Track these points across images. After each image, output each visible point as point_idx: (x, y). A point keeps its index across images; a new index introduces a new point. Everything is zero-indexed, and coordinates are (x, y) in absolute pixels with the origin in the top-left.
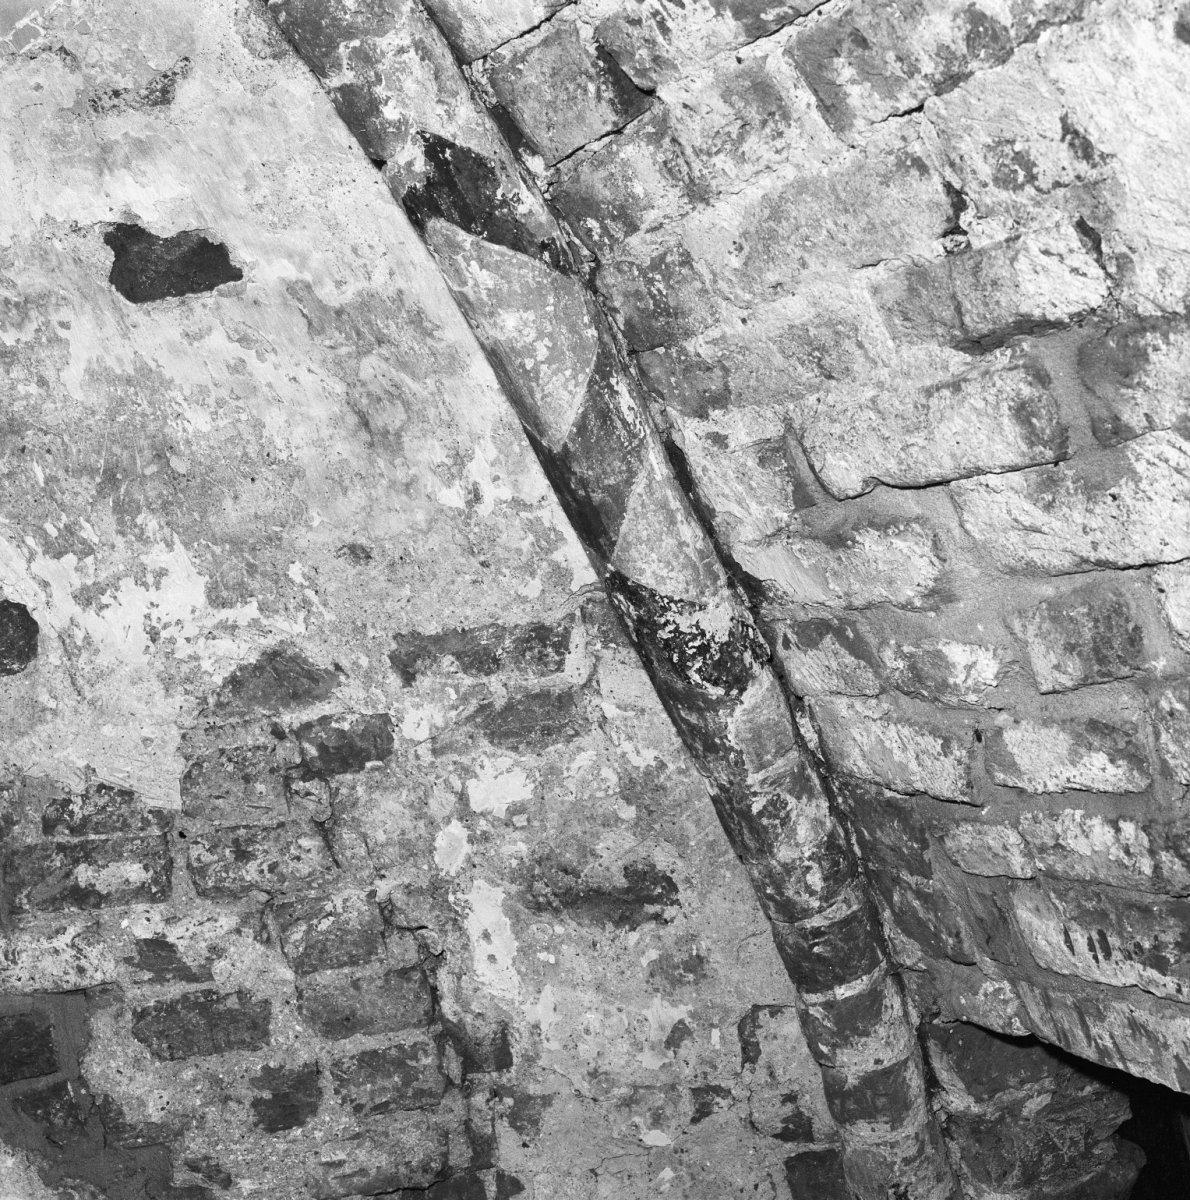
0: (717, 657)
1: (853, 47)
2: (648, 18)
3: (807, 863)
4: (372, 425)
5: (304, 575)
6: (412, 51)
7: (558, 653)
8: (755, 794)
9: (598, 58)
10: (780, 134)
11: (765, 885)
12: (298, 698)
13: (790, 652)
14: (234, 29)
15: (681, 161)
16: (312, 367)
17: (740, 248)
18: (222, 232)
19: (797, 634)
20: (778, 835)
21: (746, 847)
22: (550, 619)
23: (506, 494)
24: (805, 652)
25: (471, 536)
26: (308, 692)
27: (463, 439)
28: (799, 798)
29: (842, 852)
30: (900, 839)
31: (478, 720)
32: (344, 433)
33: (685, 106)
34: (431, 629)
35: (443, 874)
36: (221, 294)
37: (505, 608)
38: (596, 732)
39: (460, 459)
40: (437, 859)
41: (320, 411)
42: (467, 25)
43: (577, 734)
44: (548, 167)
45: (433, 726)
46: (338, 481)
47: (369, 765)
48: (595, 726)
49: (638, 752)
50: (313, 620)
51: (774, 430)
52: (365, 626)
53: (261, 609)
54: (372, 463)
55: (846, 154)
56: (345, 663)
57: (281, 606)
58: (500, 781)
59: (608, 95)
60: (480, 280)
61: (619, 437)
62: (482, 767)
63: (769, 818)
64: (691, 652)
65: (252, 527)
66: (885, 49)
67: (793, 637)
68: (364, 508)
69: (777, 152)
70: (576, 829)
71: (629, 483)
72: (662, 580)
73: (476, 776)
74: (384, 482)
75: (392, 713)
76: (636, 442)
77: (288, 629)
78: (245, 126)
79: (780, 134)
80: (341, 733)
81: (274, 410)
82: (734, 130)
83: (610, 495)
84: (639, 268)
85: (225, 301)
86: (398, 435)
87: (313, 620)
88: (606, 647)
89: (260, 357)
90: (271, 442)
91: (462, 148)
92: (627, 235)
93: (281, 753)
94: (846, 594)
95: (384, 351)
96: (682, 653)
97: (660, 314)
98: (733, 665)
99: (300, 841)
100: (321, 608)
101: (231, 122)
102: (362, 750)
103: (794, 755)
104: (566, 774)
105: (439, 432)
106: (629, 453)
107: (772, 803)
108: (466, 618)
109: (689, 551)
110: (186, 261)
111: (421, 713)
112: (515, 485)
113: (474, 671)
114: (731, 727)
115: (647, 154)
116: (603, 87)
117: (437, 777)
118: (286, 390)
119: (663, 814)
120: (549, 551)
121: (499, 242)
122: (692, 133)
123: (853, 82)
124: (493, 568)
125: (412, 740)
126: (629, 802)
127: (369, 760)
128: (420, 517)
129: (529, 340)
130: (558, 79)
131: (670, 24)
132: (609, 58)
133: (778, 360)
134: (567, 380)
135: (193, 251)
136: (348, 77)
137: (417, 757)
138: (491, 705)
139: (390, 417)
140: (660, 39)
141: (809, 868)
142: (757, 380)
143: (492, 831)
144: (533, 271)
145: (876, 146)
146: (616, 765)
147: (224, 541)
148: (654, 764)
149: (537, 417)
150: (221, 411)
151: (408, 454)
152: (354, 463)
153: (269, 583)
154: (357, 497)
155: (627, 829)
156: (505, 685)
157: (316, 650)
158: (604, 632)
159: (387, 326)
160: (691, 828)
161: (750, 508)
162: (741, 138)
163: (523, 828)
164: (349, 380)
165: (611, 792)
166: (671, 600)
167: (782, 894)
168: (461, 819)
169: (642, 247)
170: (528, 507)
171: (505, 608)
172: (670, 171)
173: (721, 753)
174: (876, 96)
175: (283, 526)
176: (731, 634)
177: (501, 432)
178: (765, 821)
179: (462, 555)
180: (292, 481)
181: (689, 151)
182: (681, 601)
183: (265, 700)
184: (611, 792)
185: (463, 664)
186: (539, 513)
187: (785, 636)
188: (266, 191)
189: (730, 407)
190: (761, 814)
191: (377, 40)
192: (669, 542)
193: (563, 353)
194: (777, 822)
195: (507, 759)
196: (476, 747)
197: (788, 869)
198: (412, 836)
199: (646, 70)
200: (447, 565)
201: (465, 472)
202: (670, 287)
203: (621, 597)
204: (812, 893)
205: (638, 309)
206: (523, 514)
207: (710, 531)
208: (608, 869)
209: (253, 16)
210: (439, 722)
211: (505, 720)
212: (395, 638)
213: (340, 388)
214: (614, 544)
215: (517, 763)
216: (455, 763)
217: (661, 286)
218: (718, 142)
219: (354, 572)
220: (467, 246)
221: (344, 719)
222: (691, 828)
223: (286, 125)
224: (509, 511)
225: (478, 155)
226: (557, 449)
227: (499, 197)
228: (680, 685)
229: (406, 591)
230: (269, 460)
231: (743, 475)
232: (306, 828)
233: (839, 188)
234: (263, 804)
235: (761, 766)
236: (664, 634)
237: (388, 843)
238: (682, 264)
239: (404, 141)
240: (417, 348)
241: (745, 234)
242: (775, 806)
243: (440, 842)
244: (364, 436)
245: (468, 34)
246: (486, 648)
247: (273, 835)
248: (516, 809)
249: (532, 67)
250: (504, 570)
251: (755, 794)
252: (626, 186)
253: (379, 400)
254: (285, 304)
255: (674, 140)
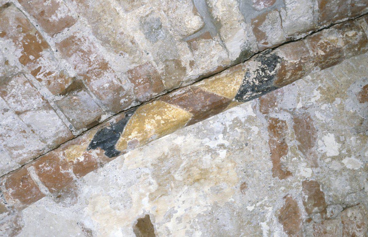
0: (266, 66)
1: (45, 16)
2: (47, 78)
3: (345, 36)
4: (198, 178)
5: (251, 206)
6: (65, 151)
7: (279, 122)
8: (317, 54)
9: (65, 95)
10: (79, 39)
11: (354, 51)
12: (296, 212)
13: (269, 42)
14: (68, 208)
15: (94, 71)
16: (179, 196)
17: (121, 53)
18: (133, 220)
19: (261, 40)
20: (333, 46)
21: (339, 57)
22: (267, 125)
23: (221, 136)
24: (267, 37)
25: (236, 148)
26: (294, 208)
27: (202, 149)
28: (320, 39)
29: (343, 24)
30: (334, 4)
31: (304, 151)
32: (201, 188)
33: (75, 69)
34: (270, 164)
35: (362, 167)
36: (154, 222)
37: (263, 139)
38: (309, 110)
39: (209, 150)
40: (357, 169)
41: (194, 195)
42: (60, 135)
43: (309, 117)
44: (105, 114)
45: (307, 166)
46: (217, 191)
47: (321, 190)
48: (306, 111)
49: (315, 96)
50: (267, 204)
51: (185, 45)
52: (269, 187)
53: (263, 222)
54: (211, 179)
55: (81, 19)
56: (283, 195)
57: (262, 214)
58: (328, 144)
59: (76, 93)
60: (135, 136)
61: (189, 95)
62: (322, 151)
63: (326, 49)
64: (263, 74)
65: (234, 221)
66: (43, 6)
67: (263, 41)
68: (227, 183)
69: (85, 40)
70: (345, 119)
71: (204, 92)
72: (237, 83)
73: (325, 153)
74: (218, 176)
75: (301, 180)
76: (192, 90)
77: (271, 213)
78: (98, 208)
79: (79, 39)
80: (309, 198)
81: (194, 210)
82: (81, 54)
83: (208, 98)
84: (135, 87)
85: (156, 222)
86: (202, 170)
87: (267, 204)
88: (277, 106)
89: (176, 212)
90: (205, 212)
91: (94, 138)
92: (124, 90)
93: (317, 220)
94: (239, 21)
95: (173, 172)
96: (264, 77)
97: (150, 81)
98: (269, 60)
99: (349, 216)
100: (263, 201)
101: (97, 212)
102: (316, 192)
103: (306, 41)
104: (324, 122)
105: (201, 156)
106: (194, 92)
107: (321, 48)
108: (266, 152)
109: (229, 74)
110: (144, 232)
111: (302, 170)
112: (218, 132)
113: (286, 151)
114: (292, 61)
115: (94, 82)
116: (73, 94)
117: (326, 166)
118: (187, 205)
119: (338, 88)
120: (241, 123)
121: (123, 129)
122: (84, 67)
123: (57, 16)
124: (248, 142)
125: (312, 174)
126: (334, 100)
127: (319, 190)
128: (230, 165)
129: (154, 122)
130: (73, 108)
131: (47, 71)
132: (65, 92)
133: (159, 43)
134: (168, 110)
135: (140, 229)
136: (70, 171)
137: (318, 173)
138: (299, 146)
139: (196, 172)
140: (53, 75)
141: (346, 35)
142: (168, 50)
143: (346, 148)
144: (133, 119)
145: (77, 9)
146: (320, 104)
147: (240, 231)
148: (319, 91)
149: (181, 121)
150: (195, 227)
151: (208, 167)
152: (212, 185)
153: (254, 218)
154: (223, 185)
155: (345, 101)
156: (291, 141)
157: (278, 204)
158: (271, 106)
159: (164, 170)
160: (343, 79)
161: (212, 55)
162: (82, 51)
163: (345, 138)
164: (183, 184)
165: (331, 106)
166: (245, 80)
167: (357, 45)
168: (342, 159)
169: (127, 86)
170: (225, 129)
171: (263, 139)
172: (98, 75)
173: (302, 65)
174: (59, 9)
175: (234, 211)
176: (259, 61)
177: (199, 136)
178: (328, 50)
179: (243, 152)
180: (218, 206)
181: (90, 68)
182: (245, 77)
183: (297, 224)
184: (331, 106)
185: (283, 155)
186: (227, 125)
187: (263, 44)
188: (120, 204)
189: (180, 60)
190: (325, 52)
191: (60, 161)
192: (225, 80)
193: (160, 111)
194: (328, 46)
195: (320, 142)
196: (314, 152)
197: (347, 42)
198: (348, 177)
199: (65, 80)
200: (247, 157)
201: (214, 149)
202: (140, 77)
203: (245, 97)
204: (356, 34)
205: (149, 88)
206: (228, 131)
207: (226, 68)
208: (360, 109)
209: (64, 202)
210: (304, 164)
211: (304, 142)
212: (274, 177)
213: (186, 188)
214: (225, 98)
215: (321, 139)
216: (320, 160)
217: (140, 80)
218: (85, 59)
219: (250, 189)
220: (124, 139)
221: (304, 197)
222: (343, 79)
223: (98, 195)
224: (227, 135)
225: (96, 134)
226: (192, 115)
227: (110, 128)
228: (276, 78)
229: (257, 172)
230: (211, 213)
231: (202, 56)
232: (344, 214)
233: (93, 21)
234: (335, 228)
235: (308, 51)
236: (257, 83)
237: (351, 185)
238: (132, 73)
239: (91, 155)
240: (171, 161)
241: (116, 52)
242: (322, 47)
243: (350, 166)
244: (202, 181)
245: (63, 135)
246: (277, 146)
247: (346, 226)
248: (338, 140)
249: (71, 116)
250: (249, 138)
251: (317, 54)
252: (106, 89)
253: (189, 175)
254: (157, 202)
255: (88, 73)
